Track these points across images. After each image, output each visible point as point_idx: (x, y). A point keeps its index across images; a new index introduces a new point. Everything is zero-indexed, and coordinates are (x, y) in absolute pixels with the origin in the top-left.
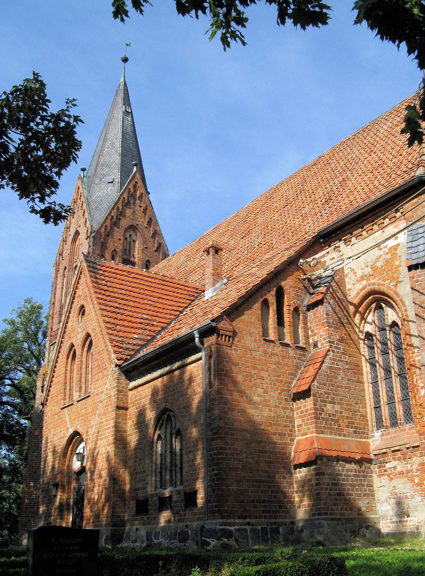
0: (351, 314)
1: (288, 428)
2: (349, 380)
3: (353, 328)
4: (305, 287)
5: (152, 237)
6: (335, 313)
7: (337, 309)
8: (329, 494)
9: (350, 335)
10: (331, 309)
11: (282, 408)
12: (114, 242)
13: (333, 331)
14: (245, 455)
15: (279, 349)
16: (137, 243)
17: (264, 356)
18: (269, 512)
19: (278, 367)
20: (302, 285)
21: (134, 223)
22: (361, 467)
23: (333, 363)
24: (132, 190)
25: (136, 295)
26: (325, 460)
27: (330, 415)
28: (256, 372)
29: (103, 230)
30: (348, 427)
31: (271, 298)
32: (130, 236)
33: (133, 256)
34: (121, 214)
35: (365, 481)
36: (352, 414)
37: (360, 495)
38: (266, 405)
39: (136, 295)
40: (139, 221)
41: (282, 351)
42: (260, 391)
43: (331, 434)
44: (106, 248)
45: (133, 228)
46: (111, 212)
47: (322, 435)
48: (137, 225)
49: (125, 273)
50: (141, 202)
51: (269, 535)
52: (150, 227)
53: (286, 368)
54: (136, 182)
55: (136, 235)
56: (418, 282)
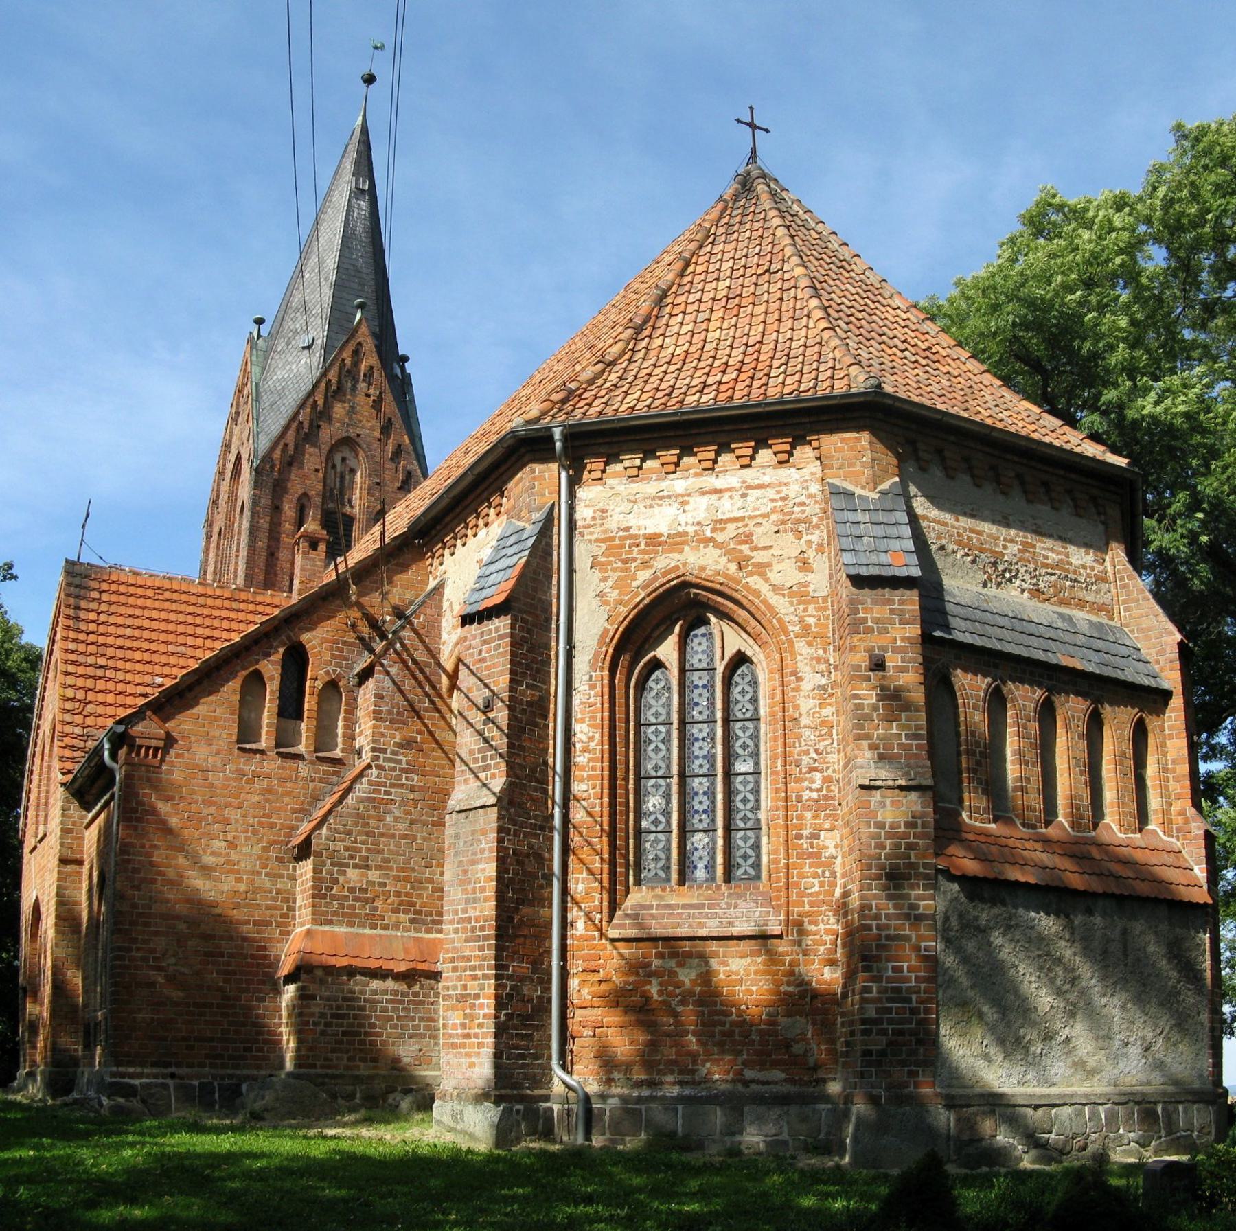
0: (444, 691)
1: (279, 913)
2: (413, 822)
3: (444, 718)
4: (361, 639)
5: (392, 459)
6: (401, 692)
7: (408, 683)
8: (323, 1033)
9: (431, 734)
10: (390, 684)
11: (267, 875)
12: (306, 477)
13: (386, 728)
14: (173, 960)
15: (272, 765)
16: (359, 474)
17: (235, 780)
18: (221, 1056)
19: (267, 800)
20: (354, 635)
21: (352, 432)
22: (409, 987)
23: (376, 792)
24: (348, 362)
25: (154, 636)
26: (319, 973)
27: (352, 890)
28: (212, 810)
29: (277, 454)
30: (396, 911)
31: (271, 668)
32: (344, 459)
33: (350, 502)
34: (322, 415)
35: (416, 1011)
36: (412, 888)
37: (400, 1036)
38: (230, 871)
39: (154, 636)
40: (362, 428)
41: (283, 768)
42: (218, 845)
43: (351, 924)
44: (285, 490)
45: (349, 443)
46: (296, 414)
47: (326, 928)
48: (359, 435)
49: (150, 593)
50: (370, 384)
51: (217, 1095)
52: (388, 437)
53: (287, 799)
54: (360, 344)
55: (357, 456)
56: (469, 648)
